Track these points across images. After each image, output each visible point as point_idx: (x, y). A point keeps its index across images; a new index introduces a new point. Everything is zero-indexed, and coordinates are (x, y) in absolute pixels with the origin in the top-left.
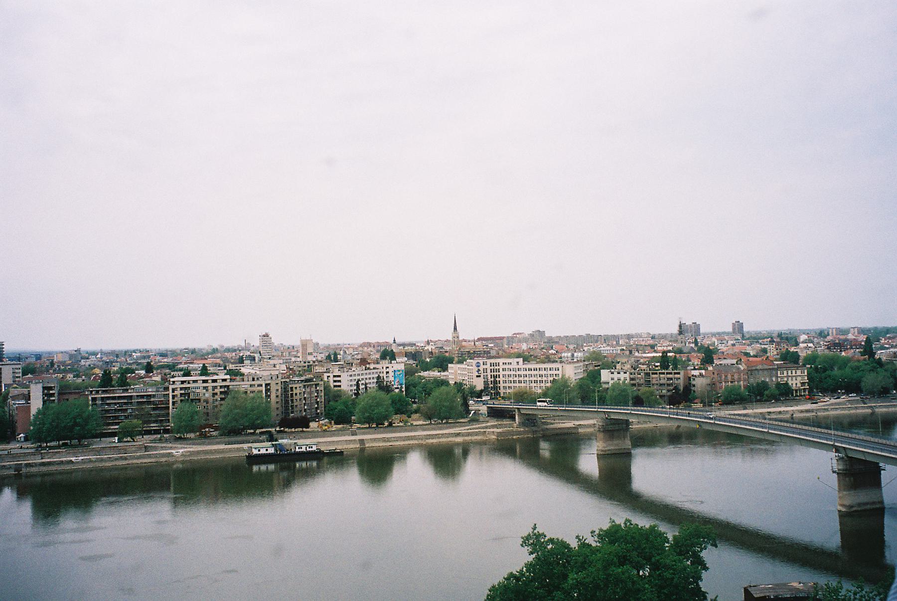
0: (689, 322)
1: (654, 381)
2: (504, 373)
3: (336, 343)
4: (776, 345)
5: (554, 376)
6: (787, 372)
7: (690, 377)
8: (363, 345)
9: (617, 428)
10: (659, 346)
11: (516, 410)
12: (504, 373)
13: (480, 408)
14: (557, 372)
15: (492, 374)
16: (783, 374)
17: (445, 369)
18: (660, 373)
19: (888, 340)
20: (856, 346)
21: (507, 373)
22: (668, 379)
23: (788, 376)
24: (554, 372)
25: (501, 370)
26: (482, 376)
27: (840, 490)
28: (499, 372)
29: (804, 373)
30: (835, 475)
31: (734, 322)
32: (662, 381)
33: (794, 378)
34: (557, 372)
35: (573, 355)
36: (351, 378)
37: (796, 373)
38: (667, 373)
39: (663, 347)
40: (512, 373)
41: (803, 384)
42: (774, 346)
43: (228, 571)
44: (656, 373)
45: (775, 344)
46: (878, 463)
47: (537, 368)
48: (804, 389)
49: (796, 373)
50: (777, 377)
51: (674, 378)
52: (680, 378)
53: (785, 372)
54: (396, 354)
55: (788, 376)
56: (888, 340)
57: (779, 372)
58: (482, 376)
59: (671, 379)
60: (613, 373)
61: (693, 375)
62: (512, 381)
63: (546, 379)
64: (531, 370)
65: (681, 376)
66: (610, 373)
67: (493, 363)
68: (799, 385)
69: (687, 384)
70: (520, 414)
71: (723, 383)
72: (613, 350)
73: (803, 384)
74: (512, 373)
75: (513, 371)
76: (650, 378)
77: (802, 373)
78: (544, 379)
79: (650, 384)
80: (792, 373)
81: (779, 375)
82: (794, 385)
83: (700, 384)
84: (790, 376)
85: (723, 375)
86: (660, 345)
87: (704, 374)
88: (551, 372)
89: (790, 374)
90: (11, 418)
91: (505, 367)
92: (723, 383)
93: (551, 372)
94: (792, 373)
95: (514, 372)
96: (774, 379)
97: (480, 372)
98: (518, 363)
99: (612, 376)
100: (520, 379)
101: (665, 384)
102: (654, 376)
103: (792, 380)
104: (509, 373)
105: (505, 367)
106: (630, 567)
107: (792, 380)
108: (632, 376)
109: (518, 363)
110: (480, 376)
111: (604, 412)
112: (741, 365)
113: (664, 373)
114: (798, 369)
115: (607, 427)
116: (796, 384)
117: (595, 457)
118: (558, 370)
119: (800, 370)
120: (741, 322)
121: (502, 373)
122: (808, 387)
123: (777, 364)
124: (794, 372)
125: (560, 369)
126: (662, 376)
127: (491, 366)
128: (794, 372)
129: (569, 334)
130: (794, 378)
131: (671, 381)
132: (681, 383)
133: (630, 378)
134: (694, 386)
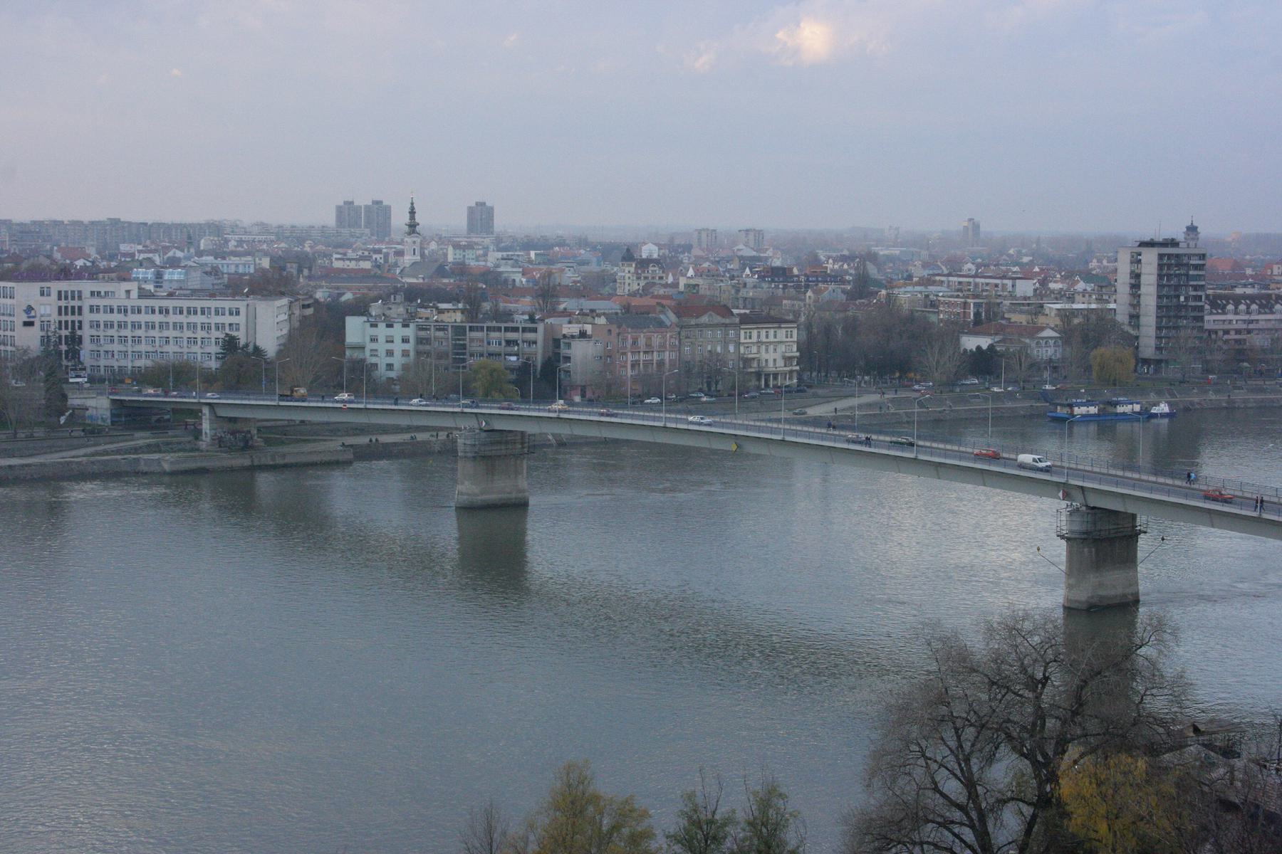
0: (362, 201)
1: (475, 348)
2: (95, 317)
4: (636, 268)
5: (227, 328)
6: (759, 332)
7: (559, 340)
9: (504, 452)
10: (337, 259)
11: (206, 410)
12: (95, 317)
13: (90, 403)
14: (234, 319)
16: (750, 338)
18: (489, 329)
19: (840, 263)
20: (817, 277)
21: (102, 317)
22: (509, 342)
23: (759, 343)
24: (227, 319)
25: (86, 310)
26: (37, 324)
27: (1070, 573)
28: (80, 313)
29: (791, 337)
30: (1064, 543)
31: (474, 205)
32: (494, 348)
33: (771, 348)
34: (234, 319)
35: (159, 276)
37: (775, 336)
38: (507, 329)
39: (348, 262)
40: (116, 317)
41: (787, 360)
42: (632, 270)
44: (482, 329)
45: (634, 265)
46: (1134, 517)
48: (791, 372)
49: (775, 336)
50: (738, 344)
51: (523, 342)
52: (535, 343)
53: (755, 333)
55: (759, 343)
56: (840, 263)
57: (742, 332)
58: (37, 324)
59: (515, 343)
60: (376, 326)
61: (565, 336)
62: (116, 339)
63: (207, 336)
65: (540, 336)
66: (368, 324)
67: (66, 292)
68: (780, 363)
69: (551, 354)
70: (217, 418)
72: (237, 266)
73: (787, 360)
74: (116, 317)
76: (464, 340)
77: (787, 337)
78: (200, 334)
79: (464, 354)
80: (767, 337)
81: (742, 340)
82: (771, 364)
83: (582, 354)
85: (629, 336)
86: (339, 256)
87: (589, 332)
88: (220, 319)
89: (763, 339)
92: (629, 354)
93: (220, 319)
94: (767, 337)
95: (122, 315)
96: (731, 348)
97: (33, 313)
98: (128, 292)
99: (373, 331)
100: (123, 333)
101: (500, 355)
104: (109, 317)
108: (423, 334)
109: (128, 292)
111: (476, 414)
112: (665, 314)
113: (499, 329)
114: (780, 327)
115: (482, 449)
116: (775, 360)
117: (453, 513)
118: (238, 313)
119: (784, 330)
120: (385, 203)
121: (87, 317)
122: (798, 368)
123: (739, 315)
125: (243, 310)
126: (494, 335)
127: (60, 298)
130: (771, 348)
131: (516, 348)
132: (539, 354)
133: (417, 338)
134: (568, 359)
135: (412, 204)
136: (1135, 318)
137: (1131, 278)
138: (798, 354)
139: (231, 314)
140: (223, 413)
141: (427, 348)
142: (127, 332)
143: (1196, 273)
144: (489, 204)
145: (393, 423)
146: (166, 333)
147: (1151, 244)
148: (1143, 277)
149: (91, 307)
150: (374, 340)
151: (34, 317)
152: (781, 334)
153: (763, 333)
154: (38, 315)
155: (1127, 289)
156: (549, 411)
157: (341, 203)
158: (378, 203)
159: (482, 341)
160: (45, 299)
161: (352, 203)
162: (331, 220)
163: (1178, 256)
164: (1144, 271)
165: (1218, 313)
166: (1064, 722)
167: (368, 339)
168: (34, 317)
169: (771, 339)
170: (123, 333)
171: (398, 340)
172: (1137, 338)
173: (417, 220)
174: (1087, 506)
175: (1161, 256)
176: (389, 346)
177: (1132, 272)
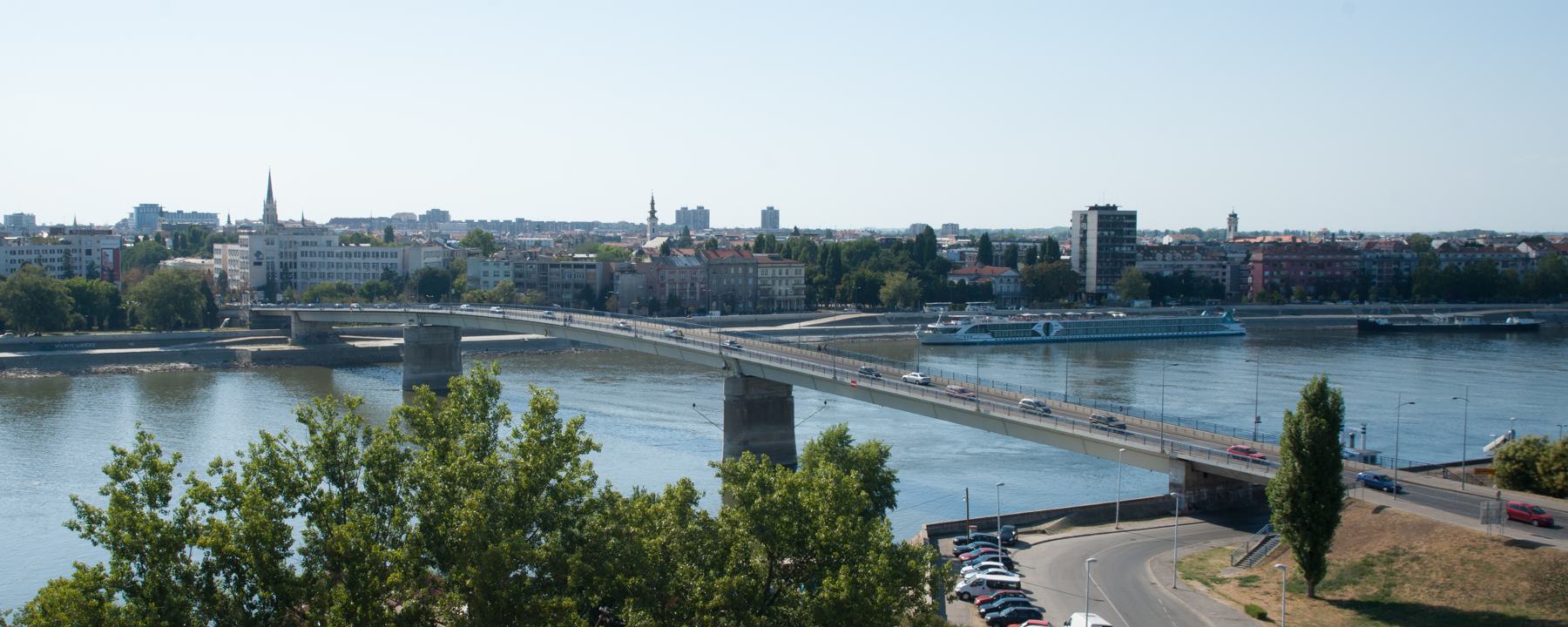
2: (305, 259)
3: (731, 226)
8: (1183, 232)
12: (305, 259)
15: (284, 261)
17: (209, 253)
21: (309, 259)
23: (774, 278)
26: (264, 263)
28: (295, 257)
33: (784, 282)
36: (13, 257)
37: (787, 273)
43: (519, 401)
47: (377, 253)
48: (798, 300)
50: (756, 278)
54: (936, 233)
55: (774, 278)
58: (264, 263)
64: (15, 253)
66: (482, 263)
71: (667, 285)
75: (320, 256)
77: (796, 274)
79: (546, 284)
80: (780, 273)
81: (759, 275)
84: (777, 278)
88: (331, 260)
89: (777, 275)
90: (1477, 249)
91: (305, 248)
94: (780, 273)
97: (261, 257)
100: (341, 270)
102: (553, 270)
103: (780, 284)
105: (305, 248)
106: (174, 582)
107: (780, 284)
110: (260, 264)
118: (396, 257)
121: (300, 259)
124: (784, 270)
126: (567, 270)
128: (784, 270)
129: (1461, 229)
130: (784, 282)
135: (653, 204)
136: (1083, 261)
137: (1081, 233)
138: (805, 286)
139: (392, 256)
140: (304, 318)
141: (522, 280)
142: (343, 270)
143: (1128, 221)
144: (775, 208)
145: (1456, 524)
146: (349, 271)
147: (1095, 208)
148: (1088, 233)
149: (302, 252)
150: (486, 274)
151: (262, 259)
152: (792, 272)
153: (777, 270)
154: (265, 258)
155: (1078, 241)
156: (488, 312)
157: (680, 209)
158: (772, 208)
159: (558, 275)
160: (269, 247)
161: (686, 208)
162: (756, 223)
163: (1115, 216)
164: (1089, 228)
165: (1149, 260)
166: (142, 530)
167: (482, 274)
168: (262, 259)
169: (784, 275)
170: (341, 270)
171: (501, 274)
172: (1085, 277)
173: (656, 209)
174: (742, 374)
175: (1100, 217)
176: (496, 279)
177: (1081, 229)
